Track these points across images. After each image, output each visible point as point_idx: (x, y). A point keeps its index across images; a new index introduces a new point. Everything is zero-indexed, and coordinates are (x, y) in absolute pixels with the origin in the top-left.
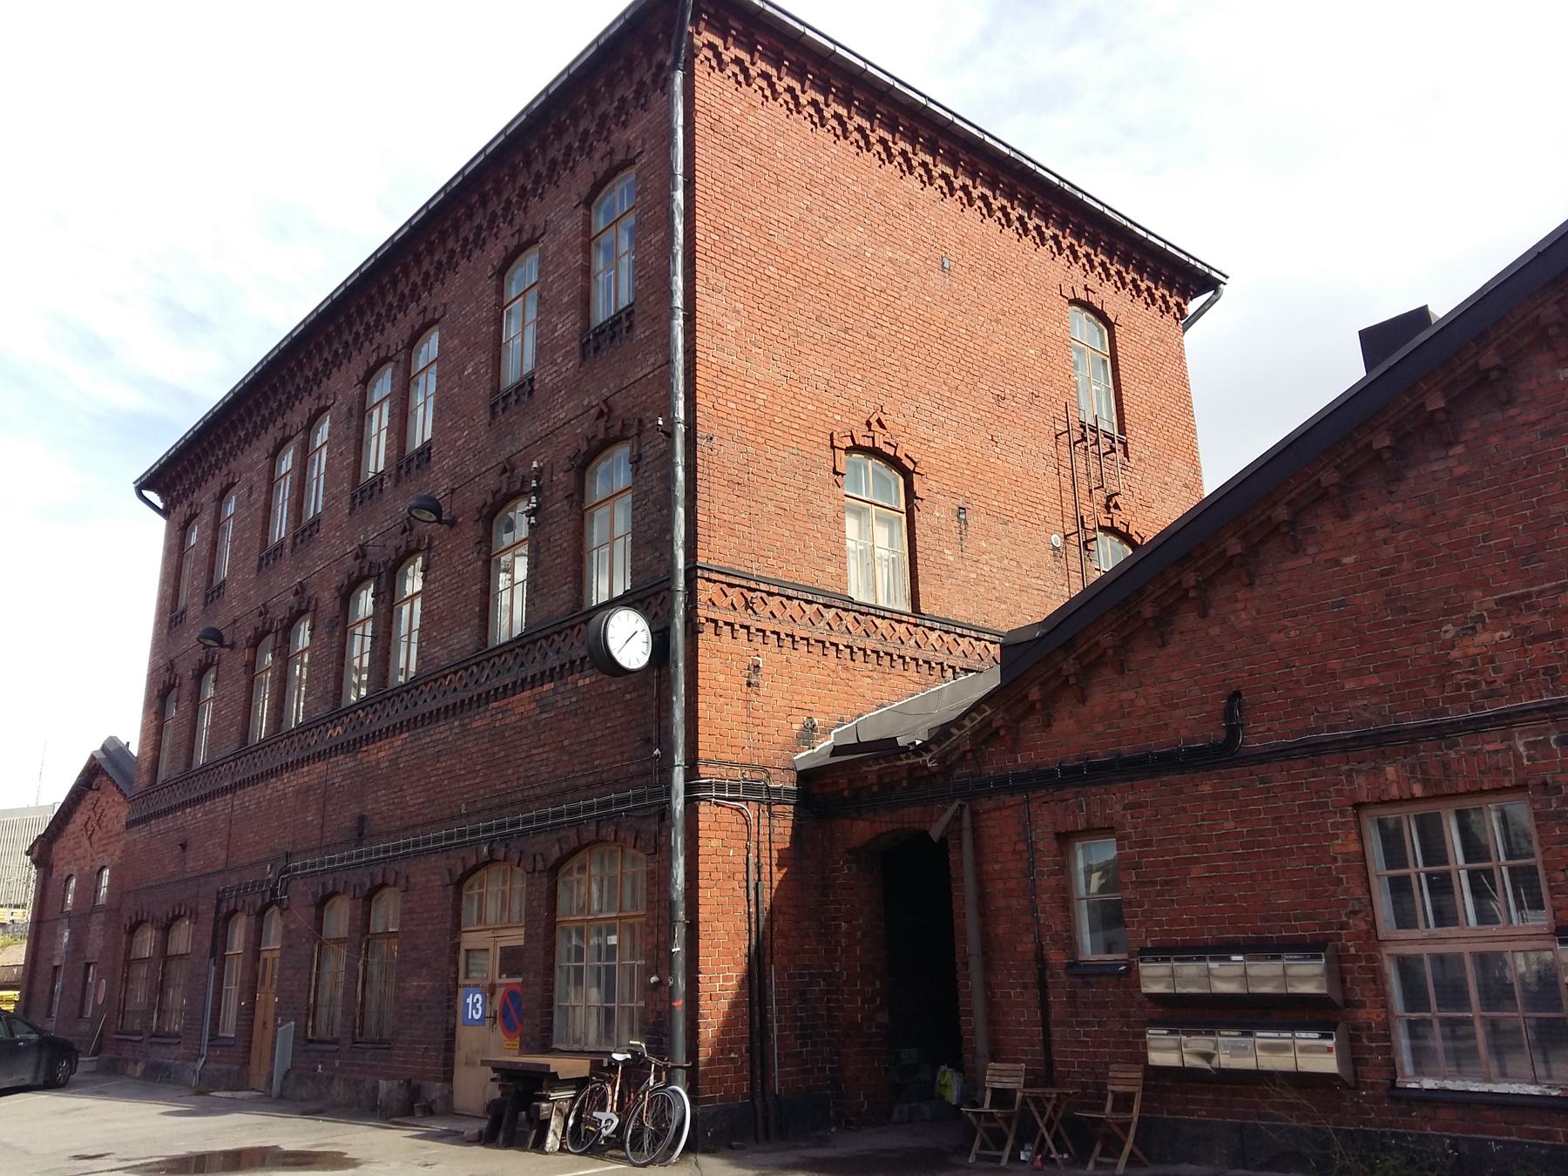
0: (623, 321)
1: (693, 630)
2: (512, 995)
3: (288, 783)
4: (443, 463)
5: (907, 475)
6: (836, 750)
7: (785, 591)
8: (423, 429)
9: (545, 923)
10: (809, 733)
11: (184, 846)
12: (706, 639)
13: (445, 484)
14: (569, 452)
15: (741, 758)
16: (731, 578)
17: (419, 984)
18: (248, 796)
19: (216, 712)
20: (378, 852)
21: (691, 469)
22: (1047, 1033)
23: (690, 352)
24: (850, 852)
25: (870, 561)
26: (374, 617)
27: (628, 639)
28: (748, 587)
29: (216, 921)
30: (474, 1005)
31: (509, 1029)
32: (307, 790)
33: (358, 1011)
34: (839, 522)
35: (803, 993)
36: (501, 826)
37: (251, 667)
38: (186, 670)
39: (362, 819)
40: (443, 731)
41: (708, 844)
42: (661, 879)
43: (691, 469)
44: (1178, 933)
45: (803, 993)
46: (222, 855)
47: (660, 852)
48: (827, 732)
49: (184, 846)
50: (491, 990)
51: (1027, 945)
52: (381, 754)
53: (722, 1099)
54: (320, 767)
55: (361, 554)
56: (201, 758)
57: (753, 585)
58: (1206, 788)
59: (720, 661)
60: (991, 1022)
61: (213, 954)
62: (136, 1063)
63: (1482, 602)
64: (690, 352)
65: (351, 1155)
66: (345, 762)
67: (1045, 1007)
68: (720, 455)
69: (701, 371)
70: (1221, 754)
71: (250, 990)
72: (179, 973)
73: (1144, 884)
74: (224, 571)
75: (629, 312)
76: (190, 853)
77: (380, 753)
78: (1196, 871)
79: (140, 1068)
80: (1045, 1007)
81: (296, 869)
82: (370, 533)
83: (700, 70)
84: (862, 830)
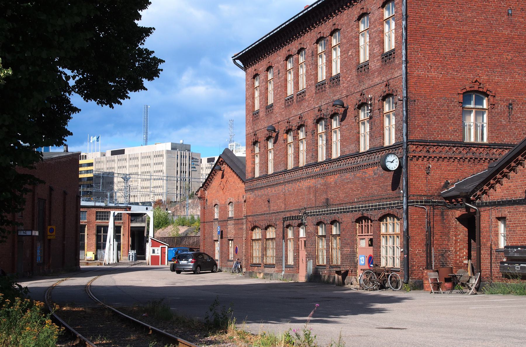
3: (305, 184)
4: (344, 84)
5: (391, 162)
7: (438, 144)
8: (336, 70)
10: (447, 185)
11: (269, 202)
13: (345, 93)
14: (379, 94)
15: (424, 193)
17: (347, 250)
18: (289, 187)
19: (275, 155)
20: (333, 210)
22: (491, 265)
24: (456, 218)
26: (395, 29)
29: (284, 228)
32: (310, 188)
33: (330, 257)
35: (442, 255)
36: (366, 207)
38: (261, 136)
39: (327, 199)
40: (349, 175)
44: (515, 242)
45: (442, 255)
46: (283, 206)
48: (452, 184)
49: (269, 202)
51: (489, 245)
52: (332, 180)
53: (418, 279)
56: (271, 171)
57: (428, 144)
58: (521, 209)
60: (33, 221)
61: (283, 239)
62: (260, 273)
65: (79, 108)
66: (321, 181)
67: (491, 259)
71: (297, 251)
72: (270, 244)
73: (510, 231)
74: (271, 101)
75: (394, 50)
76: (271, 204)
77: (331, 179)
78: (518, 228)
79: (262, 275)
80: (491, 259)
81: (308, 213)
82: (323, 103)
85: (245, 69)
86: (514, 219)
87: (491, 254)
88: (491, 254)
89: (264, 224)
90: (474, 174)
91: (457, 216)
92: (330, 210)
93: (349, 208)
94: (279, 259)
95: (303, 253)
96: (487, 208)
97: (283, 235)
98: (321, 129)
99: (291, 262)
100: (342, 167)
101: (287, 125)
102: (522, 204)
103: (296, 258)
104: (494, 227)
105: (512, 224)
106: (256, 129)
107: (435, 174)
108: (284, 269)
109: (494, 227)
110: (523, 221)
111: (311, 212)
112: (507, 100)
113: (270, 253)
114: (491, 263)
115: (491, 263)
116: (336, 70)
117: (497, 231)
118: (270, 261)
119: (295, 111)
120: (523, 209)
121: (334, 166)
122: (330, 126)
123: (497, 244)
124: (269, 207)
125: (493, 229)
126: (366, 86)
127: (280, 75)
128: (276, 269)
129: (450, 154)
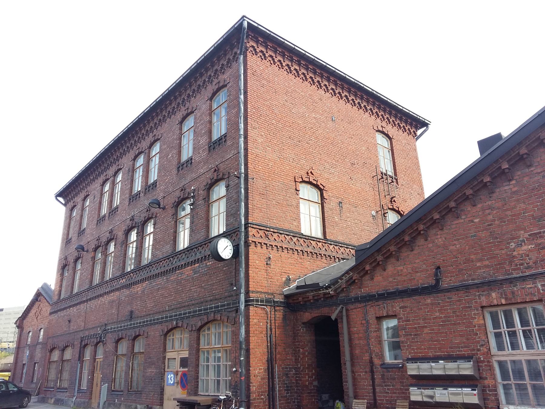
0: (222, 139)
1: (247, 245)
2: (184, 375)
3: (106, 299)
4: (161, 187)
6: (298, 287)
7: (279, 232)
9: (196, 350)
10: (288, 281)
11: (69, 321)
12: (252, 248)
13: (162, 195)
16: (260, 227)
20: (137, 323)
21: (246, 189)
22: (374, 389)
23: (246, 149)
24: (303, 323)
25: (310, 223)
27: (225, 248)
28: (266, 230)
29: (80, 348)
30: (170, 378)
31: (183, 387)
33: (130, 380)
34: (298, 207)
35: (287, 374)
36: (180, 314)
37: (94, 258)
40: (160, 281)
41: (253, 321)
42: (236, 334)
43: (246, 189)
46: (83, 324)
47: (235, 323)
48: (294, 281)
50: (176, 374)
51: (366, 357)
54: (117, 293)
55: (132, 219)
57: (268, 229)
58: (429, 301)
59: (256, 256)
61: (79, 360)
62: (52, 398)
63: (523, 235)
64: (246, 149)
66: (126, 292)
67: (373, 379)
68: (257, 184)
69: (250, 156)
70: (433, 289)
71: (92, 373)
72: (67, 367)
74: (84, 225)
76: (72, 324)
77: (138, 289)
80: (373, 379)
83: (249, 55)
84: (307, 316)
85: (65, 205)
86: (415, 317)
87: (372, 372)
88: (372, 372)
89: (62, 345)
90: (314, 272)
91: (305, 320)
92: (134, 324)
93: (158, 319)
94: (72, 383)
95: (98, 376)
96: (359, 305)
97: (79, 356)
98: (133, 236)
99: (84, 387)
100: (153, 273)
101: (96, 243)
102: (430, 293)
103: (91, 381)
104: (376, 331)
105: (411, 324)
106: (66, 254)
107: (275, 267)
108: (76, 394)
109: (376, 331)
110: (434, 318)
111: (111, 329)
112: (338, 198)
113: (66, 375)
114: (373, 385)
115: (373, 385)
116: (153, 176)
117: (380, 337)
118: (65, 384)
119: (106, 228)
120: (431, 300)
121: (144, 274)
122: (141, 233)
123: (381, 356)
124: (69, 327)
125: (373, 335)
126: (189, 179)
127: (96, 199)
128: (68, 394)
129: (292, 245)
